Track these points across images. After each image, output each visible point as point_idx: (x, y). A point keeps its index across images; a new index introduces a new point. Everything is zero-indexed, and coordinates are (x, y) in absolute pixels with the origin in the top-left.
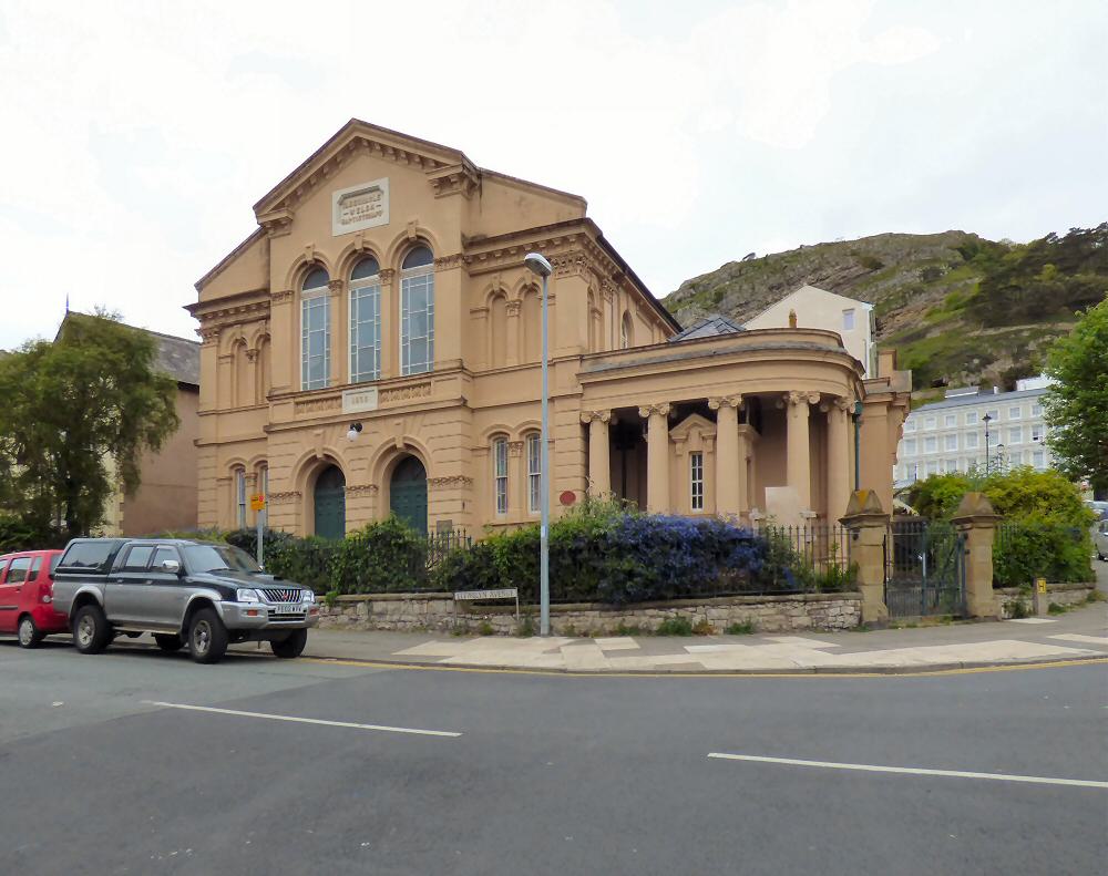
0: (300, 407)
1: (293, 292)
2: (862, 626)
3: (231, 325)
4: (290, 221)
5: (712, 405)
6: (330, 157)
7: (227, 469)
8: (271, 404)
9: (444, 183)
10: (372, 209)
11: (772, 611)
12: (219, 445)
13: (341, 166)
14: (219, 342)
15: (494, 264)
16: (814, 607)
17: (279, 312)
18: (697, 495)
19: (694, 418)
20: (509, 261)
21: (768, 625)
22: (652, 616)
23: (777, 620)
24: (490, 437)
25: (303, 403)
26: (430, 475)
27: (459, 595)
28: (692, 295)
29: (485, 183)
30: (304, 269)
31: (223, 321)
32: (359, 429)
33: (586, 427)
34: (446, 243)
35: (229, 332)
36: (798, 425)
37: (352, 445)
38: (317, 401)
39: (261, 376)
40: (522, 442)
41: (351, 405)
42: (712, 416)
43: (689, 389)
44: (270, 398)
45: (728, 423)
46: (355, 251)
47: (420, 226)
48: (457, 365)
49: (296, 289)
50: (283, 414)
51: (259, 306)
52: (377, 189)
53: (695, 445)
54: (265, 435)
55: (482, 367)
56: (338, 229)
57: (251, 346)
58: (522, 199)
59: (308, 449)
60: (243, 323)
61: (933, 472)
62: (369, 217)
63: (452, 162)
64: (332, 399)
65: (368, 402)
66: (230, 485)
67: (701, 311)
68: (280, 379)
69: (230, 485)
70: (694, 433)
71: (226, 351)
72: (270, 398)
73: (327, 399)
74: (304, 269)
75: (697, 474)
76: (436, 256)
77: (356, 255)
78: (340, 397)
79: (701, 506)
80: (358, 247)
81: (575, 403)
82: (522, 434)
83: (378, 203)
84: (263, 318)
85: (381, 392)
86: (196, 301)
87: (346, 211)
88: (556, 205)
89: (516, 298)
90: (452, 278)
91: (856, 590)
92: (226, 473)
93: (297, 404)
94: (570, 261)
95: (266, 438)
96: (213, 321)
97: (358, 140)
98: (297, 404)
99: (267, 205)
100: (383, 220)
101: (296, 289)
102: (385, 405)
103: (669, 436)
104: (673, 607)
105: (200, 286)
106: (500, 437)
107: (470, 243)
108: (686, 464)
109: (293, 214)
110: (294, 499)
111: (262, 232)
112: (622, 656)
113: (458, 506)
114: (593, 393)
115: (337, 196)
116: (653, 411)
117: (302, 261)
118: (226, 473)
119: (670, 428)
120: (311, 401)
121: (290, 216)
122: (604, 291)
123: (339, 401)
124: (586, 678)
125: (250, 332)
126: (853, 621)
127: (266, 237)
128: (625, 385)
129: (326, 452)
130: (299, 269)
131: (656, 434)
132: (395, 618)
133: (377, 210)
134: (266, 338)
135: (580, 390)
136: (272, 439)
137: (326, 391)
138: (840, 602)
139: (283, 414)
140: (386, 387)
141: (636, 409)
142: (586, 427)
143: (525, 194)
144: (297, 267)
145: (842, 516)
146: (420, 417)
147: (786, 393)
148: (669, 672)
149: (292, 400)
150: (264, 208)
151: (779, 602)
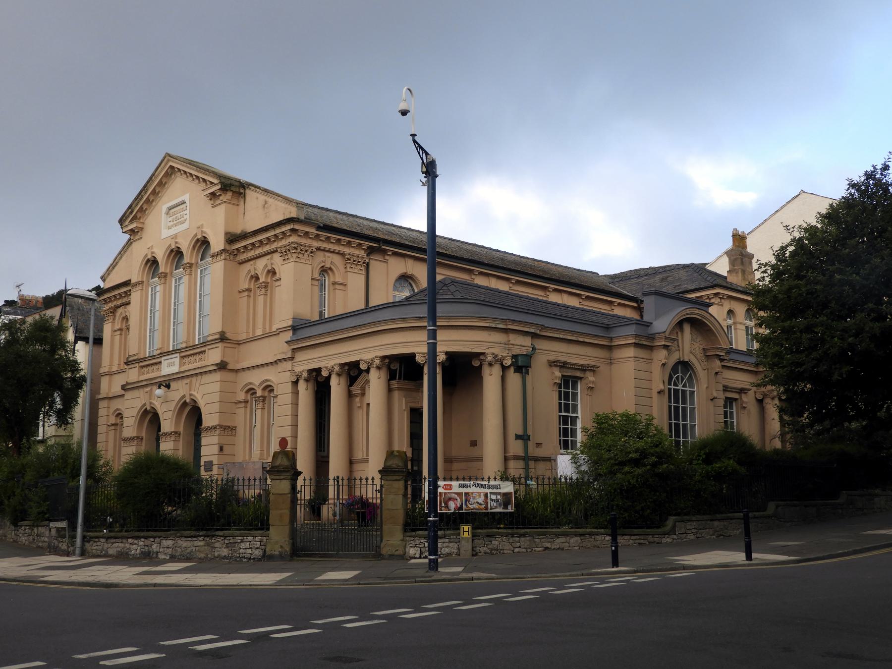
2: (266, 557)
3: (119, 307)
6: (157, 181)
7: (114, 418)
9: (213, 195)
11: (202, 543)
12: (110, 398)
13: (166, 186)
15: (251, 254)
20: (259, 251)
29: (248, 191)
30: (149, 264)
31: (115, 303)
32: (168, 386)
34: (217, 243)
35: (320, 256)
39: (124, 345)
44: (127, 363)
46: (172, 251)
48: (217, 336)
49: (144, 280)
54: (123, 392)
55: (243, 337)
58: (266, 202)
61: (603, 410)
63: (215, 181)
69: (115, 430)
71: (117, 327)
72: (127, 363)
74: (149, 264)
77: (173, 254)
78: (160, 363)
81: (288, 365)
85: (182, 357)
87: (170, 219)
92: (242, 396)
93: (182, 357)
95: (123, 395)
98: (142, 367)
102: (184, 368)
104: (142, 537)
107: (232, 238)
112: (6, 577)
114: (300, 356)
115: (164, 208)
118: (242, 396)
124: (221, 589)
126: (258, 553)
128: (334, 344)
136: (129, 395)
144: (144, 263)
146: (199, 377)
148: (191, 586)
150: (125, 220)
151: (207, 536)
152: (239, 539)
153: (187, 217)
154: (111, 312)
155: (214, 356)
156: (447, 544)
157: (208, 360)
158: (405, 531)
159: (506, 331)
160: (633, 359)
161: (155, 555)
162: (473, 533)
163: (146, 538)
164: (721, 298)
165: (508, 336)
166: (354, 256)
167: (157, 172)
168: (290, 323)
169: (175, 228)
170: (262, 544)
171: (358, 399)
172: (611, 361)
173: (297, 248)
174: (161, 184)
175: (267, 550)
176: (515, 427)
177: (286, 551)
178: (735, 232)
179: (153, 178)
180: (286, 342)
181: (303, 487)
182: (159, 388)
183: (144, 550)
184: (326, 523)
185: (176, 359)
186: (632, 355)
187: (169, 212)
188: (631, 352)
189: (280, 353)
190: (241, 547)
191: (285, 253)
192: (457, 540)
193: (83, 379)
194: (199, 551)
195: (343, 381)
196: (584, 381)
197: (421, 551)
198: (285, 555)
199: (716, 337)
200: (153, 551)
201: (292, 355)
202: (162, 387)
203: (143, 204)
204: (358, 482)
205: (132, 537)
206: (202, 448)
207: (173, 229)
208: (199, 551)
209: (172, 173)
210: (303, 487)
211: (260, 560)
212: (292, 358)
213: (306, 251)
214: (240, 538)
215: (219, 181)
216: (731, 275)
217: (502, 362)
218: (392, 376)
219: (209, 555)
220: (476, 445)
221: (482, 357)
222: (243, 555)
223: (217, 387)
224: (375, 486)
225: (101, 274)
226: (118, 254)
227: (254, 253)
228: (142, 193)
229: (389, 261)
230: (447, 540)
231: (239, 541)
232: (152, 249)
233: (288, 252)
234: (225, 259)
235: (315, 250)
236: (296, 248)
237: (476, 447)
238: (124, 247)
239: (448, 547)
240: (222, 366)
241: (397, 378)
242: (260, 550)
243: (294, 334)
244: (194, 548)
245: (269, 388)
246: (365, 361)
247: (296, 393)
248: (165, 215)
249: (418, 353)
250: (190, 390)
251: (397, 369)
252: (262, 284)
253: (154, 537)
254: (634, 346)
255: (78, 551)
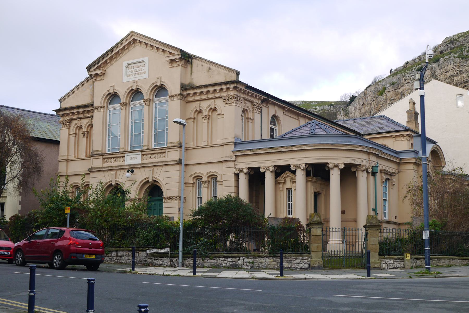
0: (106, 160)
1: (104, 106)
4: (103, 74)
5: (293, 168)
8: (92, 158)
9: (172, 61)
10: (141, 70)
11: (271, 260)
14: (70, 127)
16: (289, 259)
17: (98, 115)
18: (291, 209)
19: (288, 173)
20: (203, 97)
21: (269, 266)
22: (222, 261)
23: (273, 264)
24: (194, 178)
25: (107, 158)
26: (165, 195)
27: (149, 251)
28: (451, 49)
30: (109, 96)
32: (132, 172)
33: (237, 175)
35: (74, 122)
36: (335, 177)
37: (128, 179)
38: (114, 158)
39: (89, 144)
40: (209, 181)
41: (129, 160)
42: (294, 172)
43: (282, 160)
45: (300, 175)
46: (133, 89)
47: (162, 80)
49: (105, 105)
50: (97, 163)
51: (89, 111)
52: (143, 62)
53: (288, 185)
54: (89, 173)
55: (191, 145)
56: (125, 79)
57: (84, 129)
58: (210, 68)
59: (108, 180)
60: (81, 118)
62: (139, 74)
63: (176, 53)
64: (121, 157)
65: (136, 159)
66: (194, 122)
67: (458, 60)
68: (97, 146)
70: (288, 179)
73: (118, 157)
74: (109, 96)
75: (290, 199)
76: (170, 94)
79: (292, 215)
80: (134, 88)
81: (232, 164)
82: (208, 177)
83: (143, 68)
84: (90, 117)
85: (143, 155)
86: (59, 108)
87: (130, 70)
88: (226, 72)
89: (207, 114)
90: (176, 104)
91: (310, 254)
93: (104, 159)
94: (231, 99)
96: (67, 117)
97: (135, 40)
98: (104, 159)
99: (93, 66)
100: (146, 76)
101: (105, 105)
102: (145, 161)
103: (276, 181)
105: (61, 101)
106: (199, 178)
107: (184, 87)
108: (284, 196)
109: (105, 71)
110: (191, 185)
111: (91, 77)
113: (177, 210)
114: (240, 160)
115: (125, 64)
116: (267, 169)
117: (109, 92)
119: (276, 178)
120: (111, 158)
121: (104, 72)
122: (255, 109)
123: (123, 158)
124: (311, 281)
125: (84, 122)
126: (306, 266)
127: (91, 81)
129: (117, 182)
130: (107, 96)
131: (269, 178)
132: (126, 258)
133: (143, 71)
134: (91, 126)
135: (234, 158)
136: (93, 175)
137: (118, 153)
138: (301, 258)
139: (97, 163)
140: (145, 153)
141: (259, 168)
142: (237, 175)
143: (211, 67)
145: (364, 224)
146: (160, 168)
147: (328, 163)
149: (101, 157)
152: (294, 259)
153: (147, 70)
154: (68, 122)
155: (174, 155)
156: (399, 262)
157: (167, 158)
158: (380, 255)
159: (369, 153)
160: (413, 170)
161: (240, 267)
162: (411, 257)
163: (233, 257)
164: (409, 137)
165: (369, 156)
166: (257, 103)
167: (122, 42)
168: (233, 140)
169: (134, 77)
170: (308, 261)
171: (281, 186)
172: (399, 171)
173: (237, 98)
174: (124, 49)
175: (311, 264)
176: (372, 206)
177: (321, 265)
178: (411, 100)
179: (119, 44)
180: (232, 151)
181: (326, 232)
182: (128, 172)
183: (232, 264)
184: (335, 251)
185: (139, 156)
186: (412, 169)
187: (128, 66)
188: (411, 167)
189: (224, 157)
190: (296, 262)
191: (226, 100)
192: (403, 260)
193: (433, 180)
194: (269, 264)
195: (273, 175)
196: (390, 181)
197: (388, 266)
198: (321, 267)
199: (441, 160)
200: (239, 264)
201: (235, 158)
202: (129, 172)
203: (107, 59)
204: (331, 230)
205: (223, 257)
206: (164, 209)
207: (132, 77)
208: (269, 264)
209: (133, 43)
210: (326, 232)
211: (306, 269)
212: (235, 161)
213: (239, 100)
214: (295, 258)
215: (180, 53)
216: (409, 124)
217: (367, 170)
218: (308, 174)
219: (276, 267)
220: (345, 213)
221: (358, 167)
222: (297, 267)
223: (177, 174)
224: (362, 233)
225: (60, 97)
226: (76, 87)
227: (201, 97)
228: (108, 53)
229: (269, 107)
230: (399, 260)
231: (294, 259)
232: (114, 87)
233: (229, 99)
234: (181, 99)
235: (243, 99)
236: (236, 98)
237: (344, 214)
238: (82, 83)
239: (399, 264)
240: (179, 162)
241: (311, 176)
242: (307, 264)
243: (235, 147)
244: (267, 263)
245: (213, 177)
246: (295, 165)
247: (237, 180)
248: (126, 68)
249: (331, 163)
250: (153, 175)
251: (311, 170)
252: (207, 116)
253: (240, 257)
254: (414, 164)
255: (180, 264)
